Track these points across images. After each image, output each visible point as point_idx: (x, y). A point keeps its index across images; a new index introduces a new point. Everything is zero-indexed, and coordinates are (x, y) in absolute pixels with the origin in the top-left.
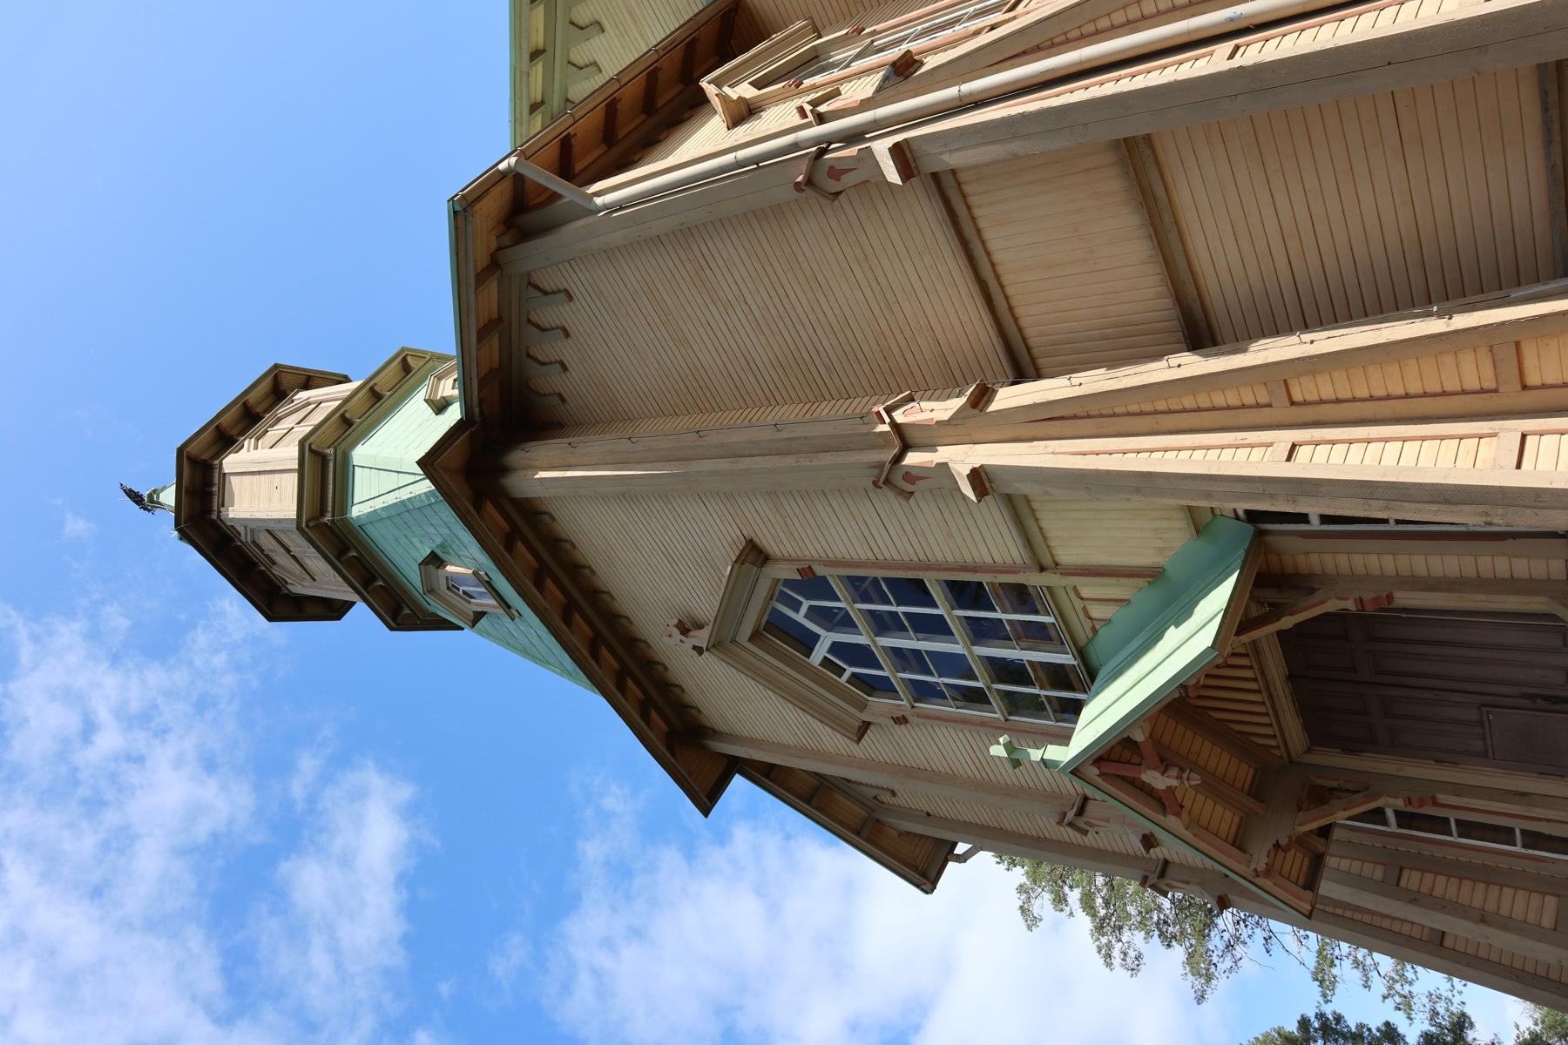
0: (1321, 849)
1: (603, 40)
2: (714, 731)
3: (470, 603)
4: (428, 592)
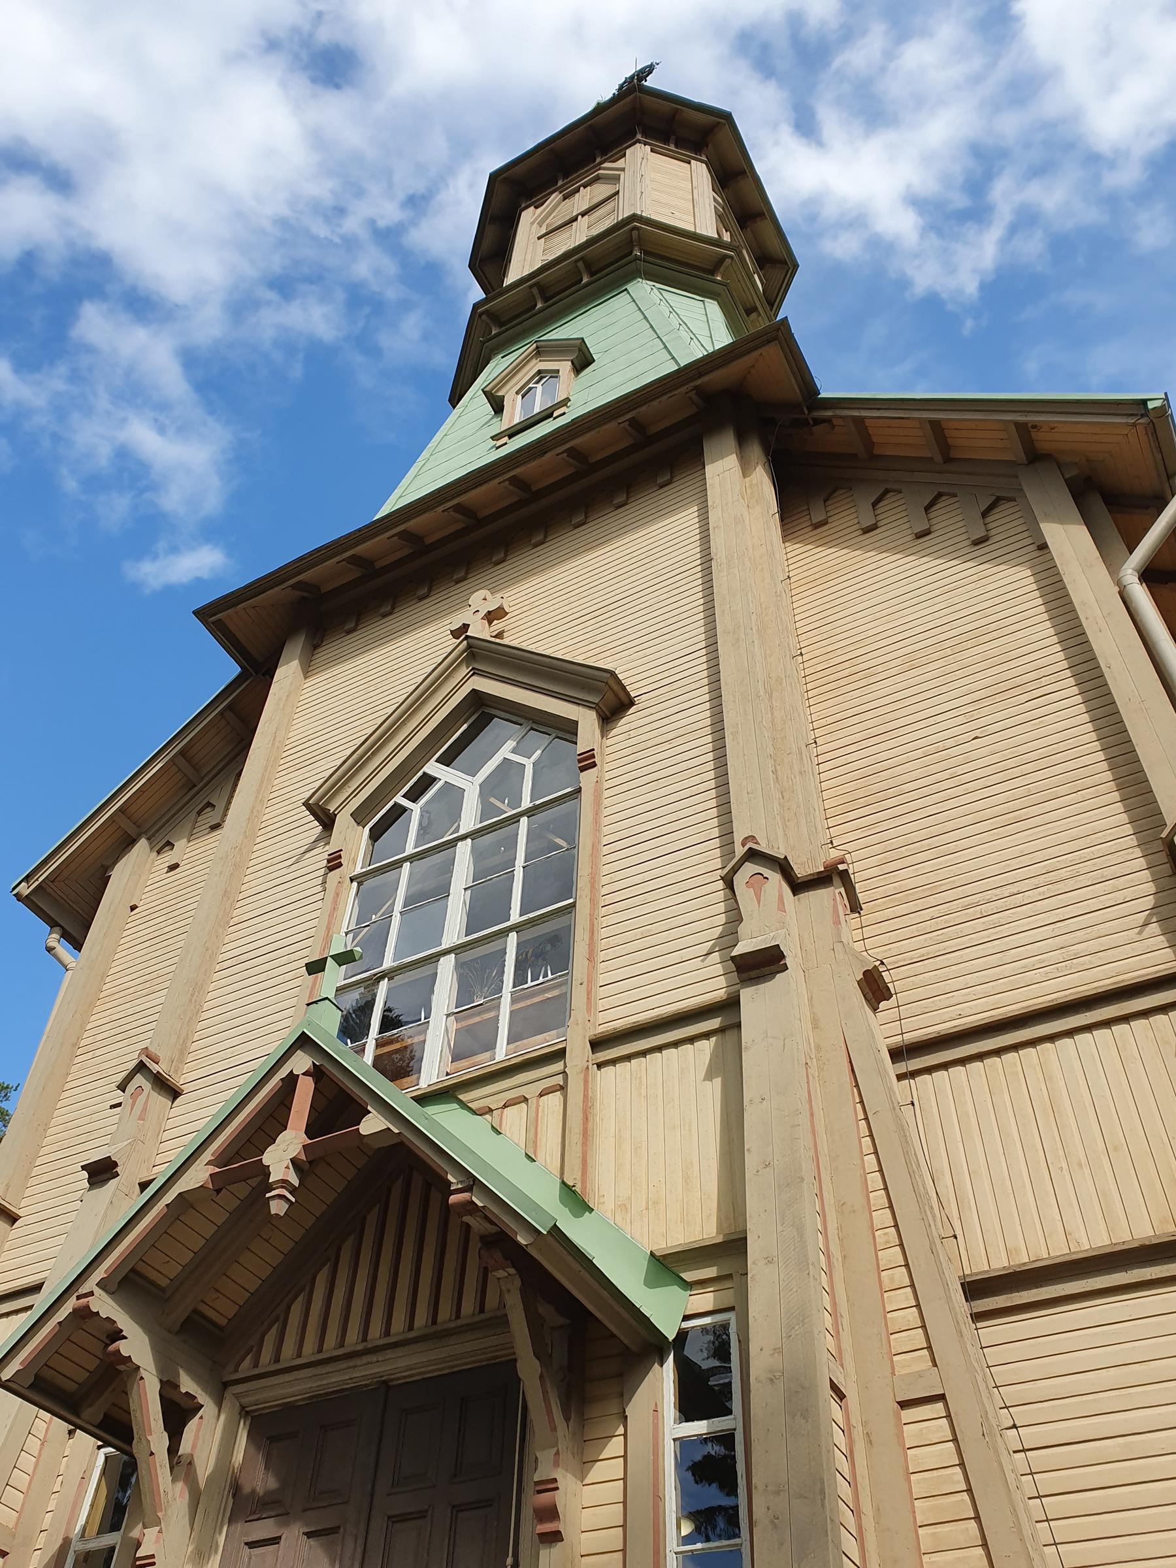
0: (87, 1413)
1: (1087, 738)
2: (316, 647)
3: (517, 393)
4: (537, 347)
